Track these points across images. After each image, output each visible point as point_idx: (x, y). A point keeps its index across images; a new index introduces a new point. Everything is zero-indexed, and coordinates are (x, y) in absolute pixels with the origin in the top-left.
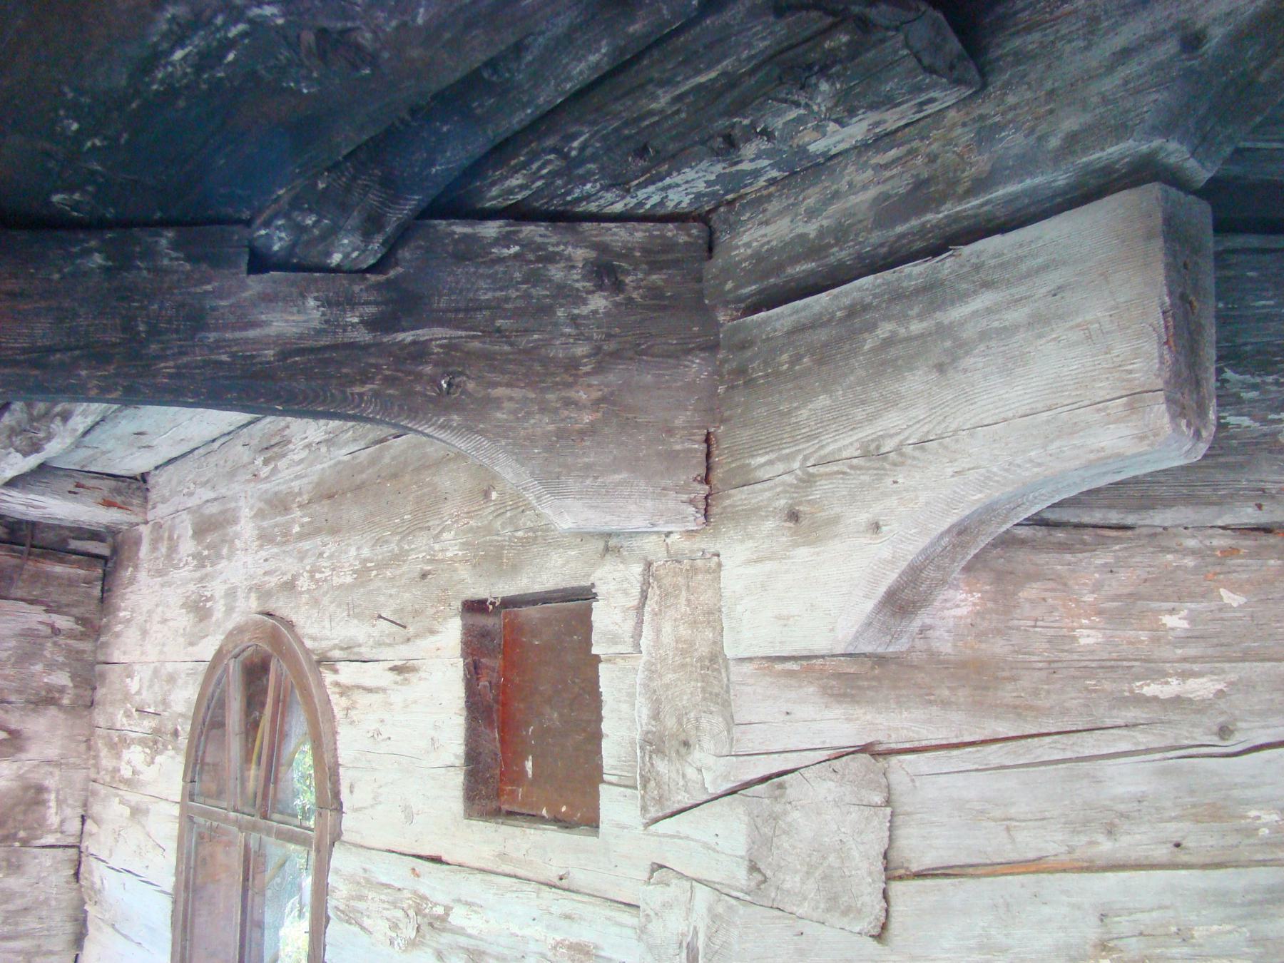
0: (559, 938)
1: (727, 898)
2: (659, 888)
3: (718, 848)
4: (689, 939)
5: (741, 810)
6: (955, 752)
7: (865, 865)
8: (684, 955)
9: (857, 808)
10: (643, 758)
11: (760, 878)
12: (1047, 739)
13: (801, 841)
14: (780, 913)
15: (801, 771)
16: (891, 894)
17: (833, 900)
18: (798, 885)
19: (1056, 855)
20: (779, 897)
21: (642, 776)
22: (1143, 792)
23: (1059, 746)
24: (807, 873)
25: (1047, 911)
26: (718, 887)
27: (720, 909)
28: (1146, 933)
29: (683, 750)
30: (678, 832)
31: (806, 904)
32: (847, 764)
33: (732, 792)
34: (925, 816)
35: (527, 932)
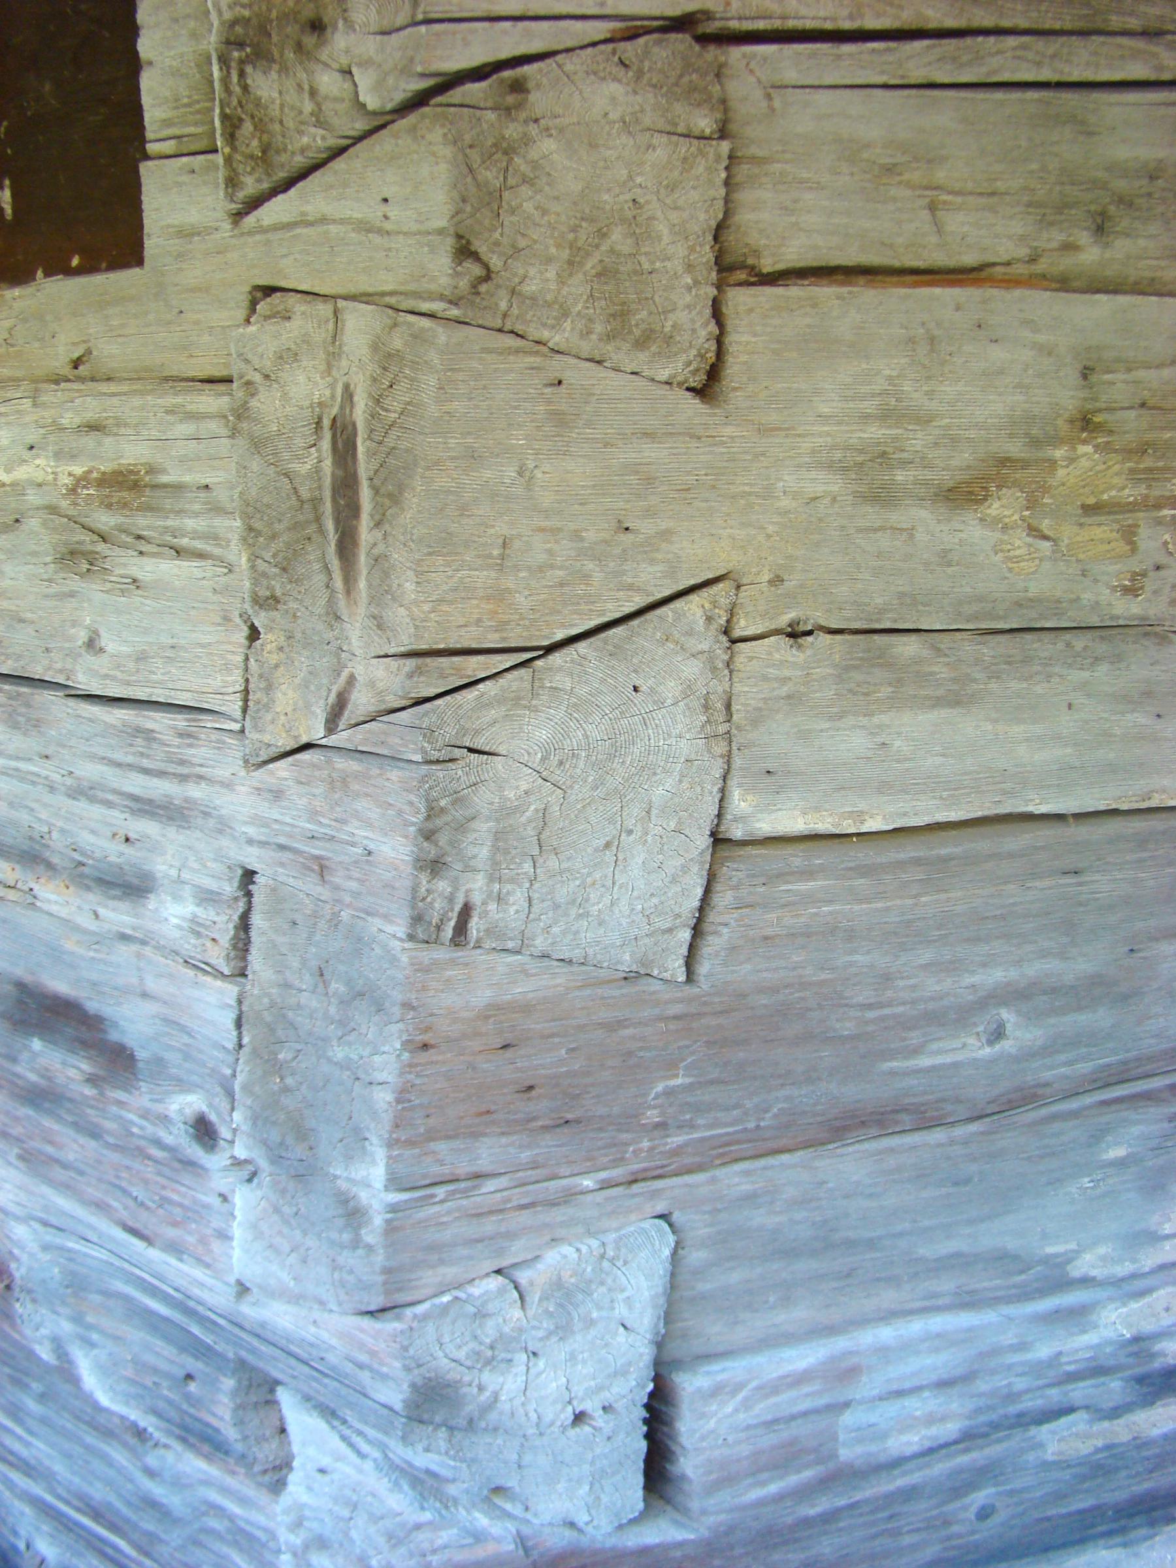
0: (78, 470)
1: (411, 318)
2: (271, 327)
3: (388, 226)
4: (335, 411)
5: (437, 135)
6: (847, 48)
7: (680, 250)
8: (326, 444)
9: (664, 139)
10: (225, 81)
11: (477, 270)
12: (1012, 41)
13: (557, 198)
14: (519, 343)
15: (559, 58)
16: (727, 310)
17: (620, 315)
18: (553, 286)
19: (1008, 264)
20: (515, 311)
21: (224, 117)
22: (1161, 161)
23: (1030, 55)
24: (570, 263)
25: (998, 354)
26: (392, 300)
27: (397, 342)
28: (1151, 403)
29: (309, 40)
30: (303, 214)
31: (567, 325)
32: (647, 52)
33: (420, 100)
34: (788, 167)
35: (21, 473)
